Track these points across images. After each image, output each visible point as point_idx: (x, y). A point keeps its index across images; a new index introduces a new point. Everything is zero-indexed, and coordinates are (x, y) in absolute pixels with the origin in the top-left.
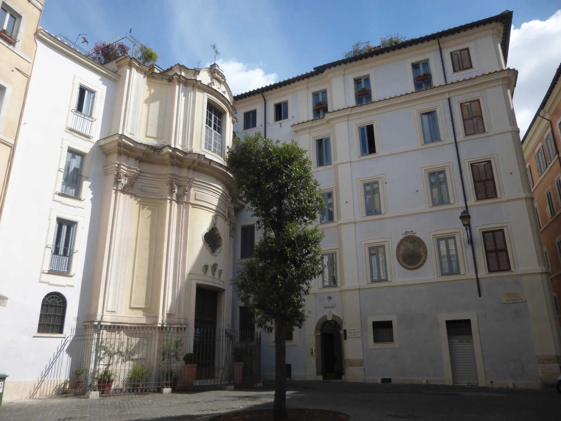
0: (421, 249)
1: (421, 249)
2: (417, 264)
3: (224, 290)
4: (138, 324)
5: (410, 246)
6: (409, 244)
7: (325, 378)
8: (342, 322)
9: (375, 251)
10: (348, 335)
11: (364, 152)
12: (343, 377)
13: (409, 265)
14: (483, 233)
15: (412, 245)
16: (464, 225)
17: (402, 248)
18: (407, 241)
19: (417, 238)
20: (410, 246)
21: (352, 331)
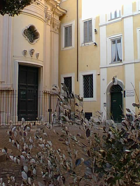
21: (129, 92)
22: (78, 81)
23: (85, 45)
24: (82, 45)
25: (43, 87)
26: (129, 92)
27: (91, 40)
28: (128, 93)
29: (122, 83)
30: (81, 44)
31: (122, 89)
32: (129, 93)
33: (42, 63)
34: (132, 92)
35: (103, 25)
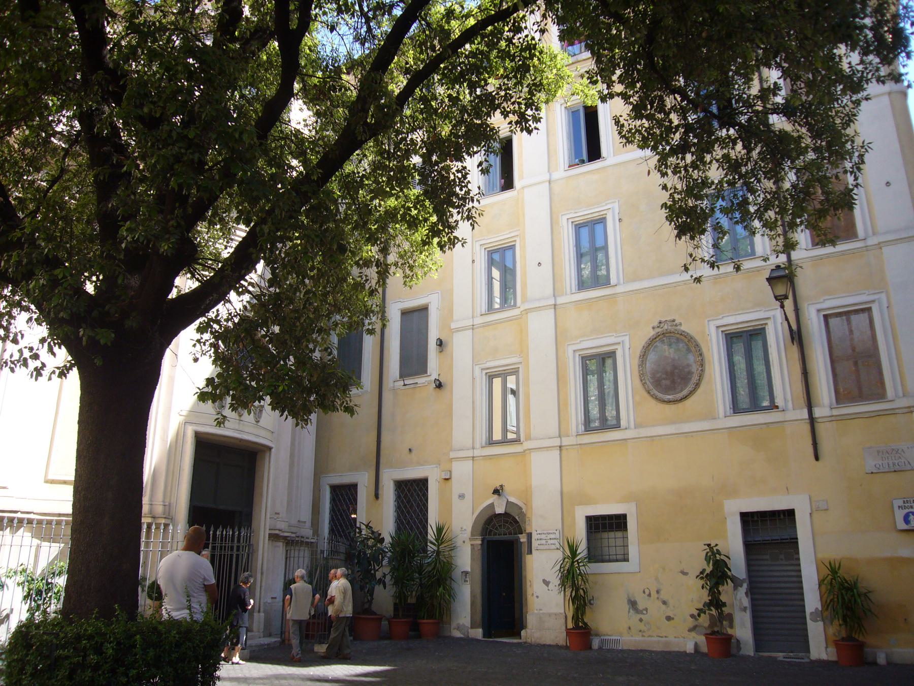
0: (691, 358)
1: (691, 358)
2: (682, 391)
3: (270, 449)
4: (60, 515)
5: (668, 351)
6: (666, 347)
7: (487, 634)
8: (523, 515)
9: (599, 363)
10: (535, 544)
11: (577, 161)
12: (523, 633)
13: (666, 393)
14: (826, 317)
15: (672, 350)
16: (776, 298)
17: (652, 357)
18: (663, 341)
19: (683, 334)
20: (668, 351)
21: (543, 536)
22: (377, 496)
23: (405, 385)
24: (396, 384)
25: (268, 516)
26: (543, 536)
27: (422, 369)
28: (539, 542)
29: (521, 508)
30: (391, 380)
31: (519, 527)
32: (543, 542)
33: (268, 435)
34: (552, 536)
35: (464, 329)
